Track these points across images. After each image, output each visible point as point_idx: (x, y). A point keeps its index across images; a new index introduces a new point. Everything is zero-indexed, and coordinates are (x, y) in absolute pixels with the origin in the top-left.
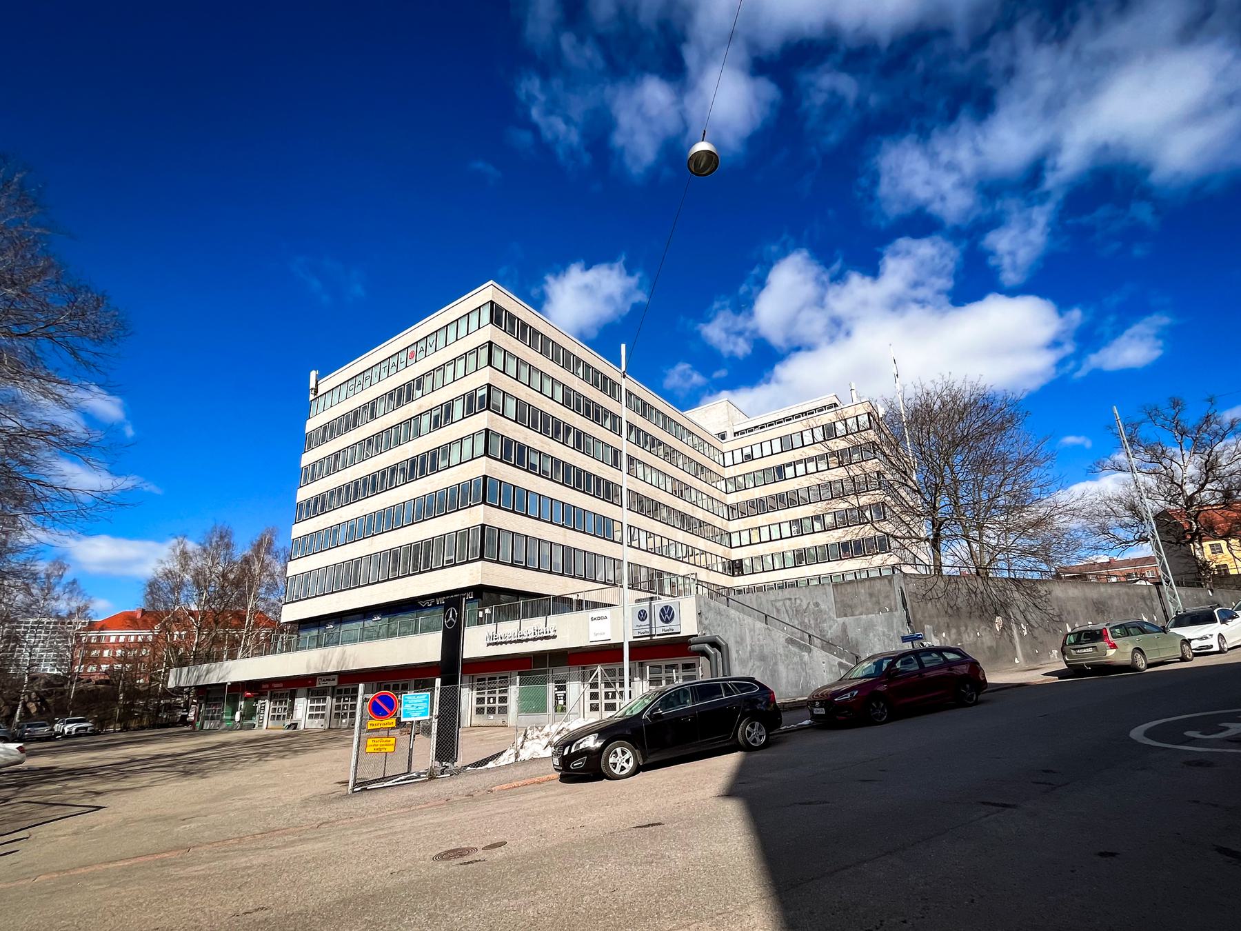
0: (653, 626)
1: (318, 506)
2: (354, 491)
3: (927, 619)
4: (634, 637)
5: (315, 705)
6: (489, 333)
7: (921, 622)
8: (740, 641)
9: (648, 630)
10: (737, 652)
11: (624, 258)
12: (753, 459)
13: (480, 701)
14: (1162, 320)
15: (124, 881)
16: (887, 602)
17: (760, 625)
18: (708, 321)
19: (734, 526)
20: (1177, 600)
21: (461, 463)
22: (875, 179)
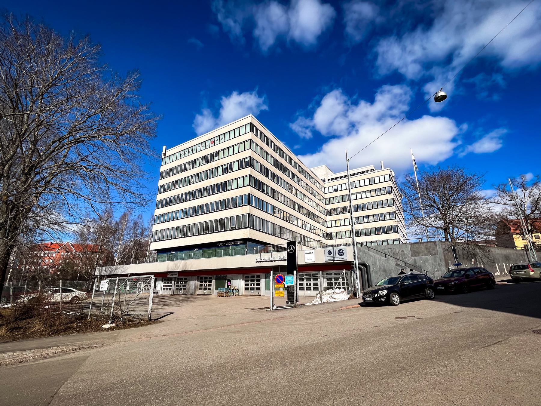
0: (335, 257)
1: (168, 202)
2: (186, 197)
3: (449, 259)
4: (326, 261)
5: (166, 284)
6: (250, 135)
7: (447, 260)
8: (375, 264)
9: (333, 258)
10: (373, 268)
11: (257, 89)
12: (338, 191)
13: (247, 285)
14: (504, 131)
15: (154, 339)
16: (434, 252)
17: (383, 258)
18: (293, 122)
19: (329, 218)
20: (535, 256)
21: (237, 188)
22: (376, 56)
